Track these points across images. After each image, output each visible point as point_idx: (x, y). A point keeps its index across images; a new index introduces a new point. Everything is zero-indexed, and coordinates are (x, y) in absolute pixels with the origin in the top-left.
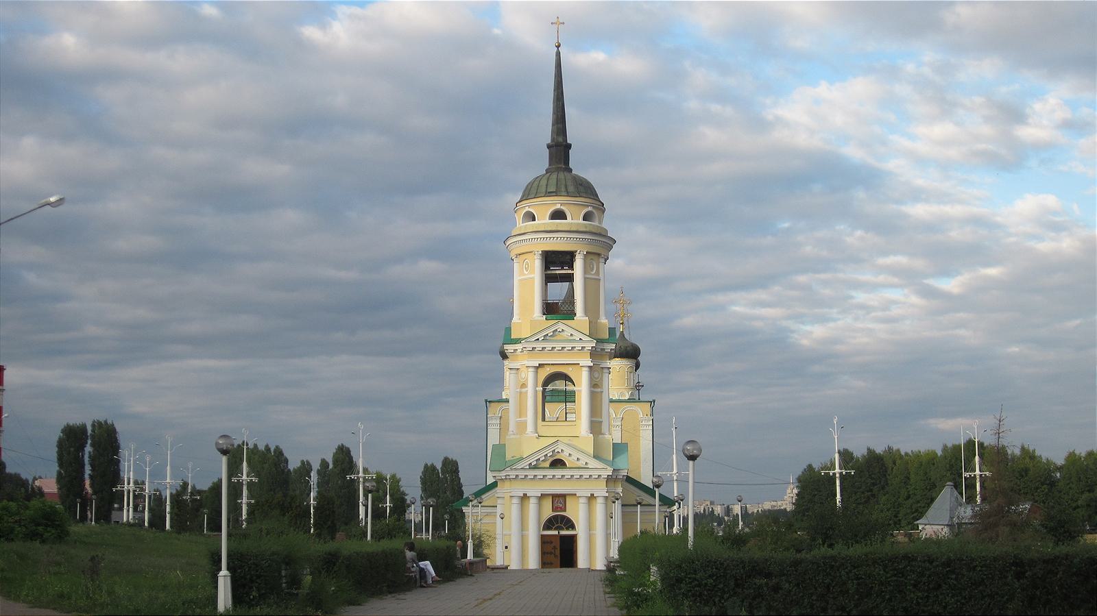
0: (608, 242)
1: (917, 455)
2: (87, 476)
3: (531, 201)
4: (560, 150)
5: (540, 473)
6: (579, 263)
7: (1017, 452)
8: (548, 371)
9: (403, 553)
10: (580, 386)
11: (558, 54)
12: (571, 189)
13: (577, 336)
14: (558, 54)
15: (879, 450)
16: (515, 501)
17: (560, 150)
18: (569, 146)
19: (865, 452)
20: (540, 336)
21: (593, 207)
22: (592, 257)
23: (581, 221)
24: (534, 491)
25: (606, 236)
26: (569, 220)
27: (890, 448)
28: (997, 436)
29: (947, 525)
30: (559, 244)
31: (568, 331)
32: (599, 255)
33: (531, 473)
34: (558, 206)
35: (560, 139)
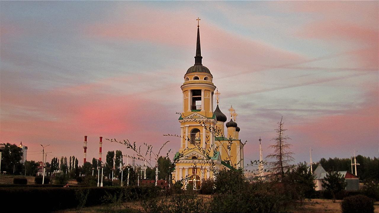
0: (205, 85)
1: (344, 160)
2: (114, 165)
3: (190, 73)
4: (198, 59)
5: (188, 161)
6: (202, 93)
7: (373, 159)
8: (192, 128)
9: (213, 185)
10: (202, 133)
11: (198, 29)
12: (200, 70)
13: (201, 117)
14: (198, 29)
15: (333, 158)
16: (181, 170)
17: (198, 59)
18: (202, 58)
19: (329, 159)
20: (189, 117)
21: (208, 76)
22: (206, 91)
23: (203, 80)
24: (186, 167)
25: (213, 85)
26: (200, 80)
27: (336, 158)
28: (279, 133)
29: (318, 180)
30: (196, 87)
31: (198, 115)
32: (210, 91)
33: (185, 161)
34: (207, 76)
35: (198, 55)
